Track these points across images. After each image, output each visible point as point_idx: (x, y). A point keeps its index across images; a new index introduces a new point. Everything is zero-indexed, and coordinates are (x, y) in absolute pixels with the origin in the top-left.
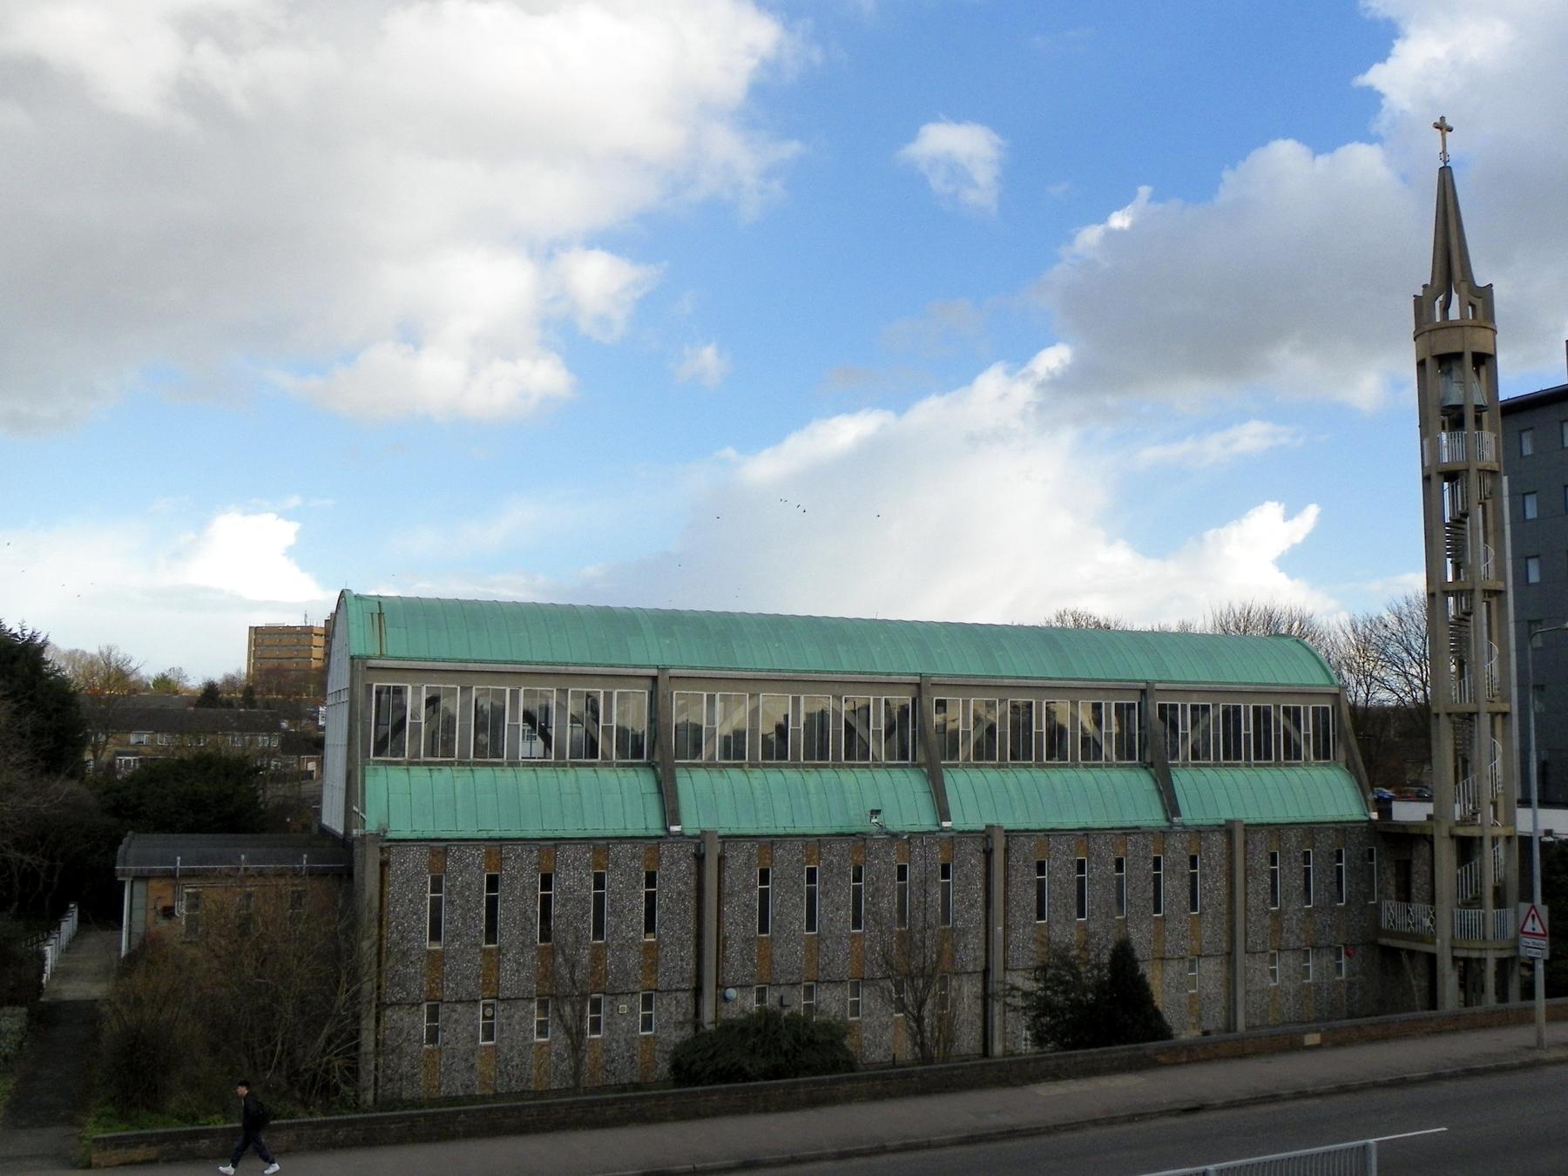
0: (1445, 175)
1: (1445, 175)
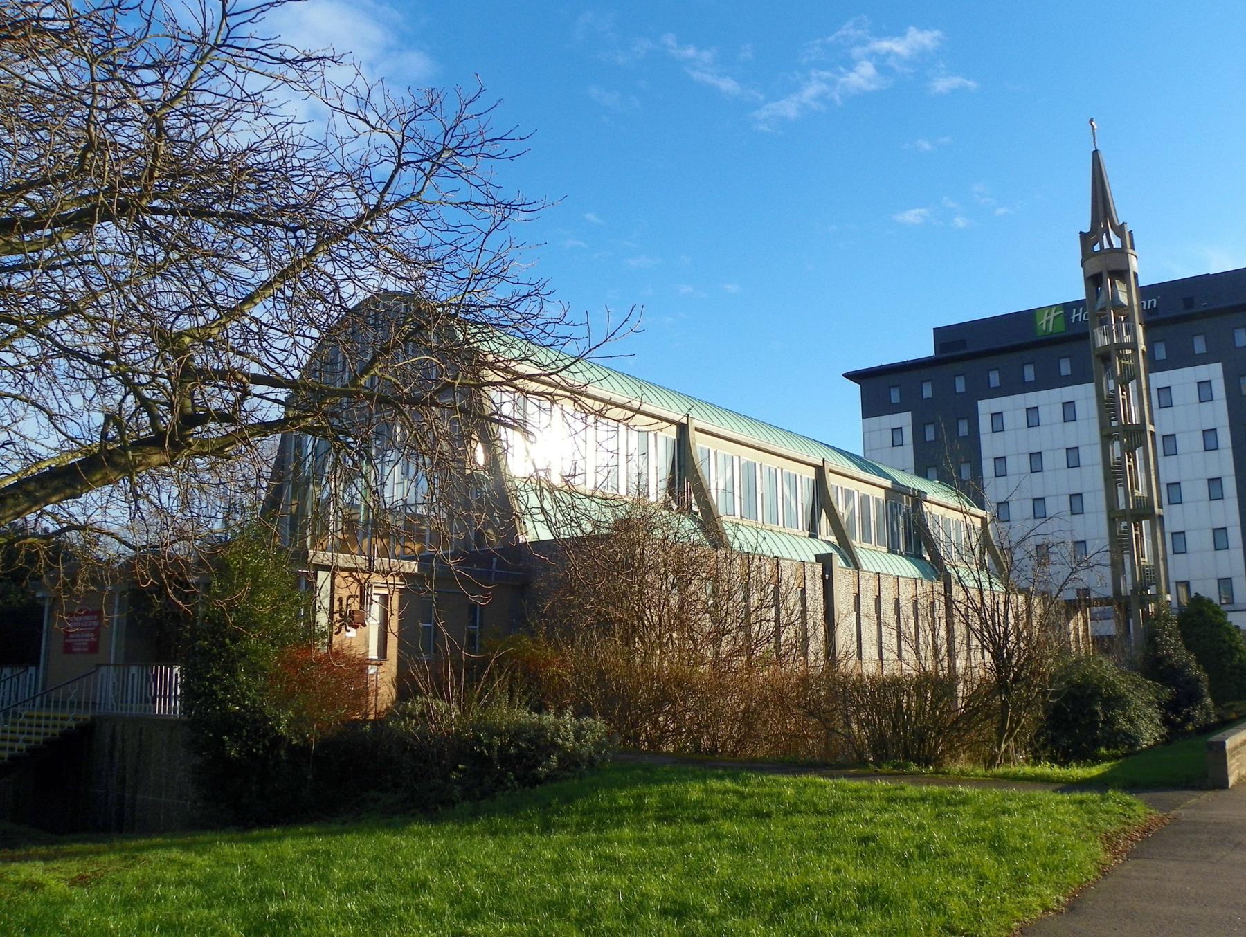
0: (1096, 154)
1: (1096, 154)
